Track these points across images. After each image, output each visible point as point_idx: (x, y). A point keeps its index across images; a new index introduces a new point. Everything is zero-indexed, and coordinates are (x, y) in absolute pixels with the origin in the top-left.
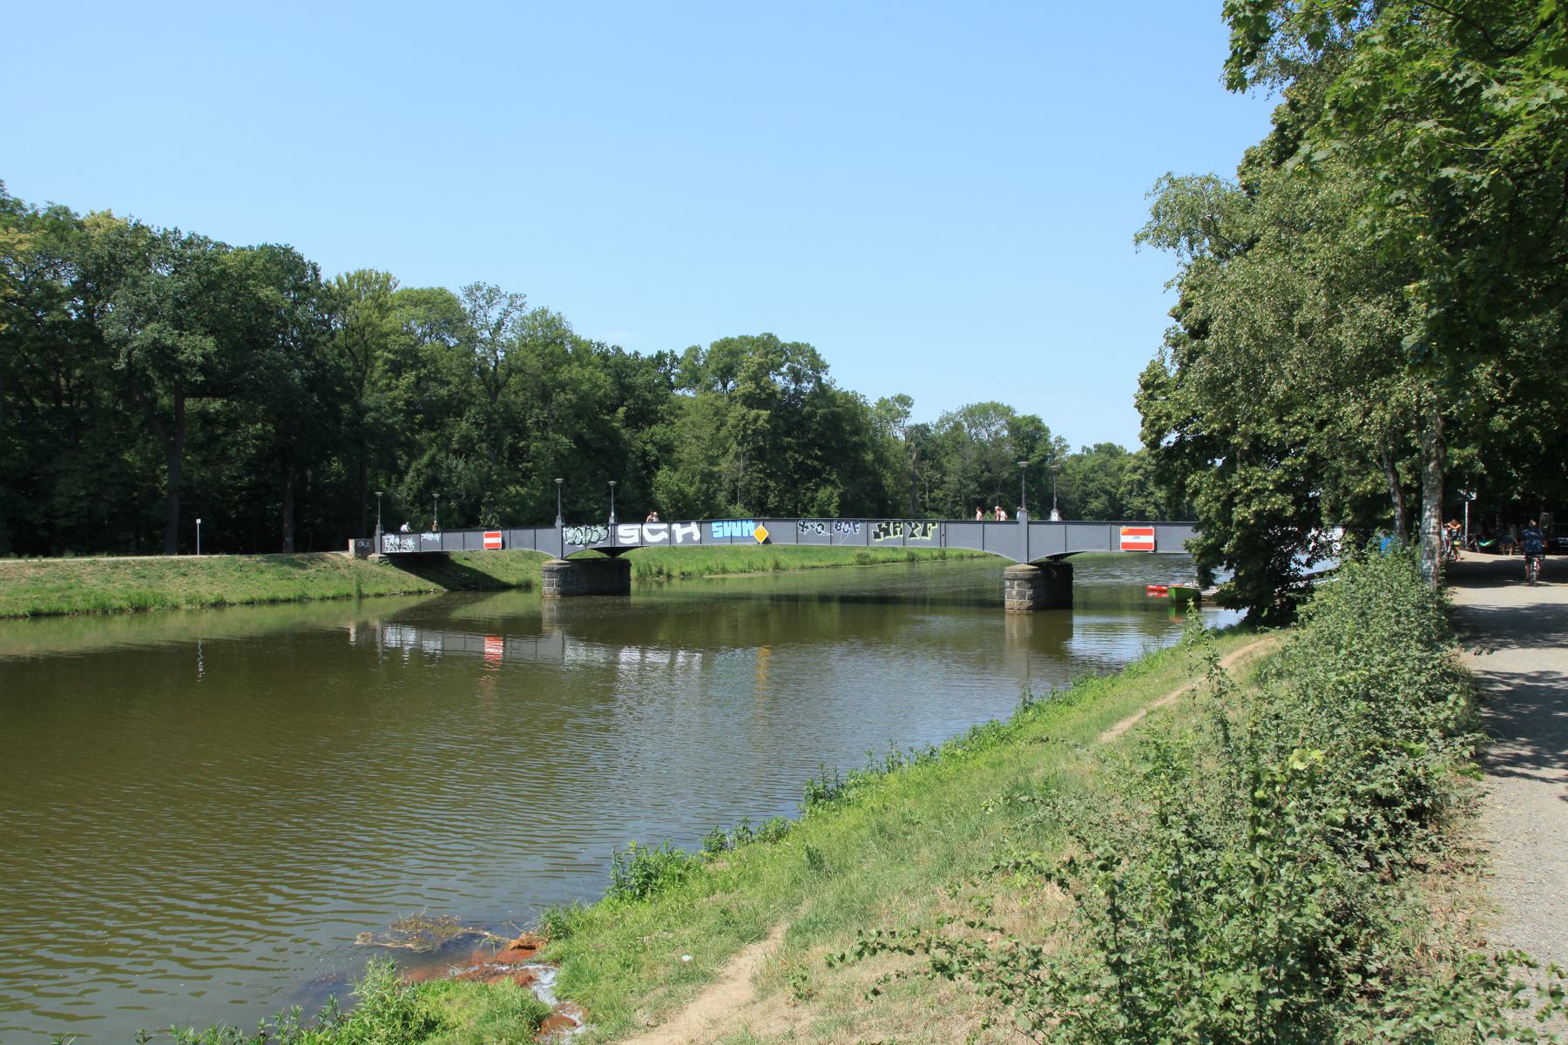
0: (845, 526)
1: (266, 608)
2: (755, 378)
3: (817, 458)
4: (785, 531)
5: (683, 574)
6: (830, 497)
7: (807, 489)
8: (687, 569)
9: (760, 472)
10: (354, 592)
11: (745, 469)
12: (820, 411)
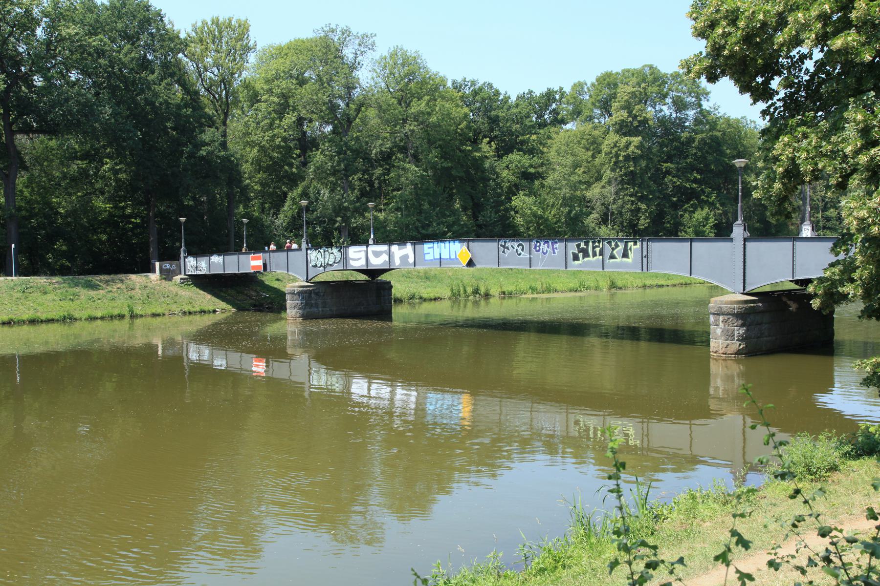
0: (544, 246)
1: (25, 328)
2: (628, 107)
3: (695, 181)
4: (486, 249)
5: (504, 293)
6: (707, 219)
7: (686, 210)
8: (508, 288)
9: (631, 196)
10: (125, 311)
11: (617, 193)
12: (699, 136)
